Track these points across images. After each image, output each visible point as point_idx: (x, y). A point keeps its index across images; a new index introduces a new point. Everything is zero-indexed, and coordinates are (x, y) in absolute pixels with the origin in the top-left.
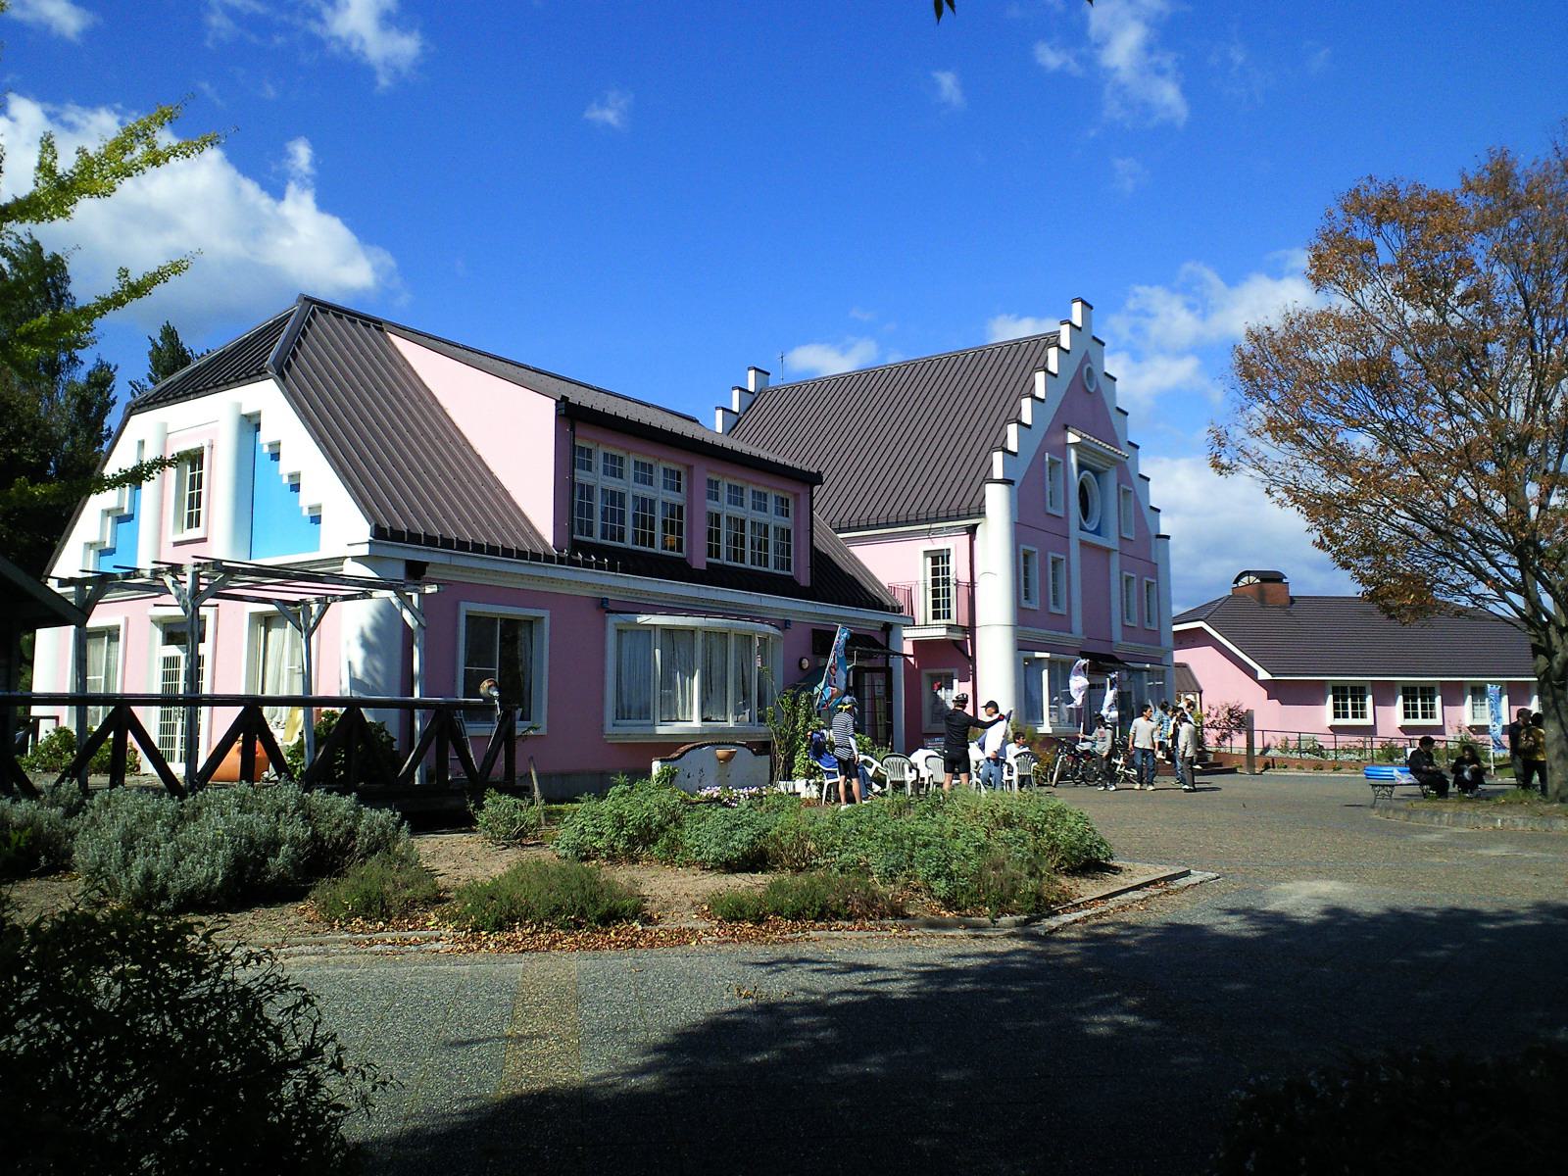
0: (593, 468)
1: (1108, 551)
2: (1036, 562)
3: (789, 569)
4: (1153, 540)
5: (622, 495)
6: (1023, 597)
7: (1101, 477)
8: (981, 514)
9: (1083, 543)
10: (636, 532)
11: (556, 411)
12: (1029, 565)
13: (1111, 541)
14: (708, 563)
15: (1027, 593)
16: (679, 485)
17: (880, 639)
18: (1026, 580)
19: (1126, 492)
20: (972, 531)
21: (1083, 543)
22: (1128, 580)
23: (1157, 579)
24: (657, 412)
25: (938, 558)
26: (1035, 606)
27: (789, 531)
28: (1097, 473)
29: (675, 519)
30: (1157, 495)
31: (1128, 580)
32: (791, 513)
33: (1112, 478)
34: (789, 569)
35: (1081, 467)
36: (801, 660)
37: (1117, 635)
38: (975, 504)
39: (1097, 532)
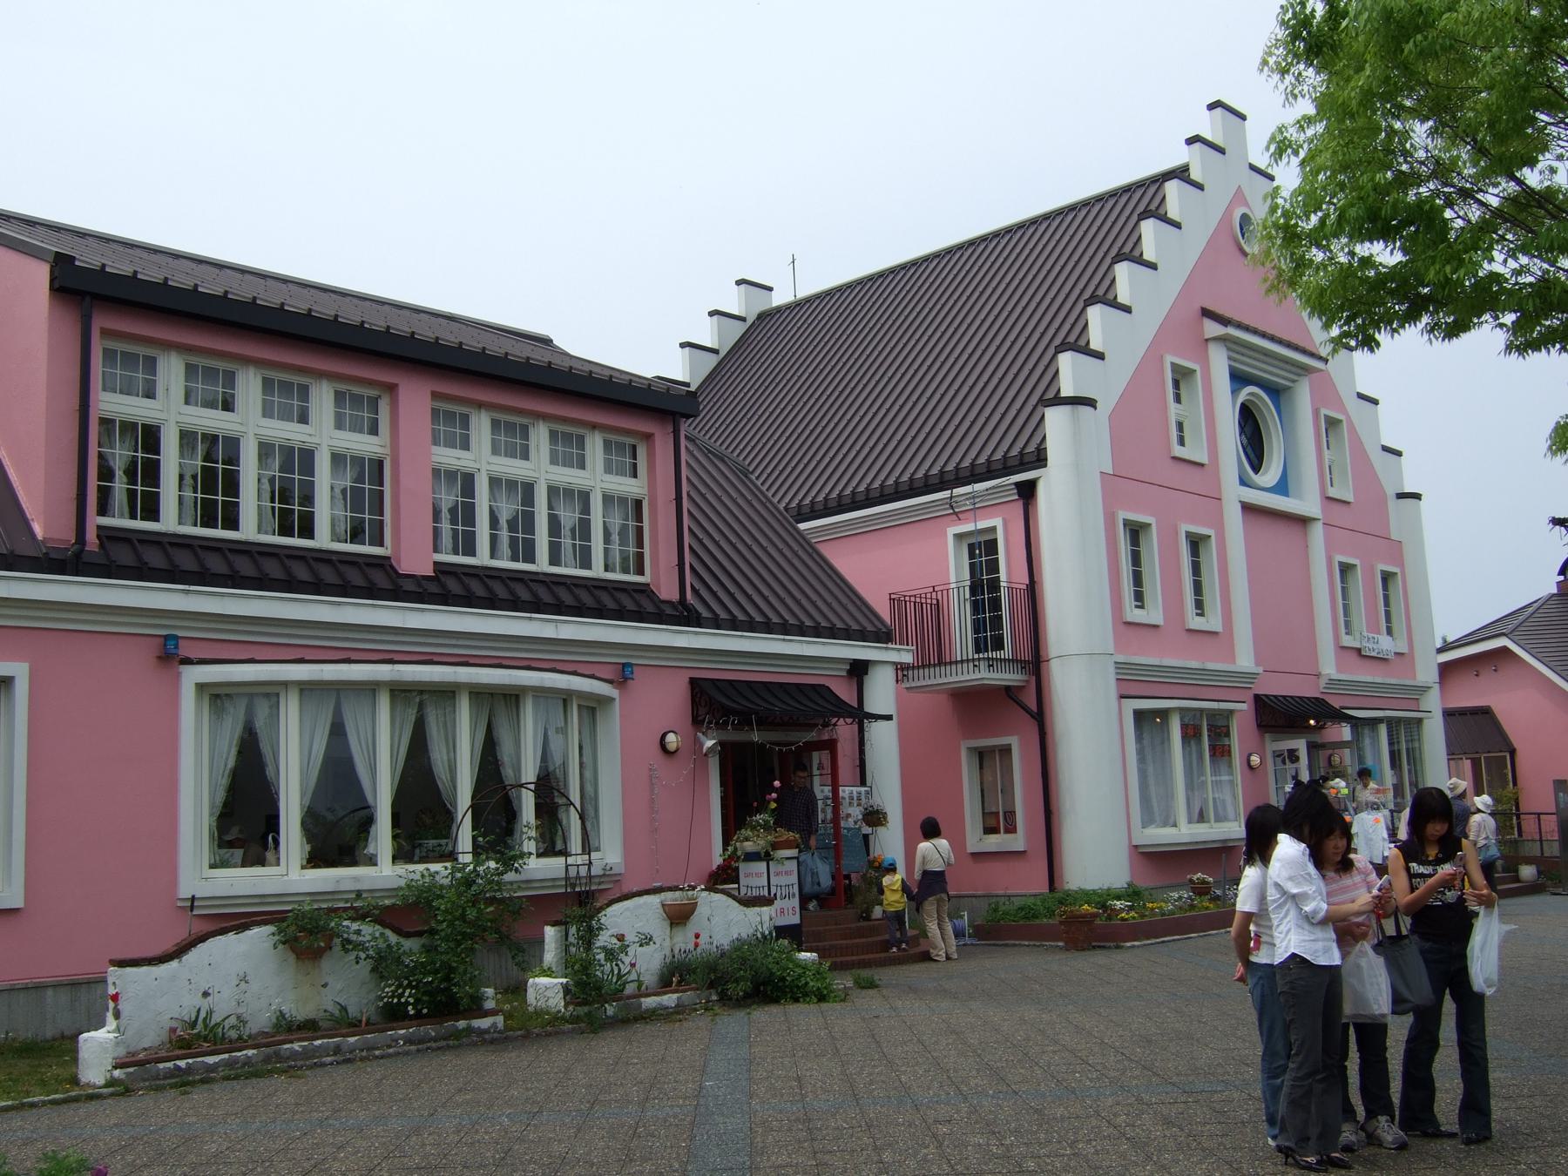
0: (160, 391)
1: (1303, 521)
2: (1152, 547)
3: (641, 572)
4: (1393, 504)
5: (233, 444)
6: (1343, 630)
7: (1282, 399)
8: (1040, 459)
9: (1247, 508)
10: (455, 532)
11: (52, 281)
12: (1203, 559)
13: (1306, 503)
14: (435, 563)
15: (1347, 624)
16: (635, 466)
17: (845, 692)
18: (1346, 607)
19: (1332, 423)
20: (1027, 492)
21: (1247, 508)
22: (1346, 569)
23: (1402, 566)
24: (209, 268)
25: (983, 550)
26: (1153, 614)
27: (381, 463)
28: (1276, 392)
29: (367, 479)
30: (1390, 427)
31: (1136, 532)
32: (384, 426)
33: (1303, 397)
34: (641, 572)
35: (1239, 379)
36: (664, 735)
37: (1329, 667)
38: (1031, 448)
39: (1282, 488)
